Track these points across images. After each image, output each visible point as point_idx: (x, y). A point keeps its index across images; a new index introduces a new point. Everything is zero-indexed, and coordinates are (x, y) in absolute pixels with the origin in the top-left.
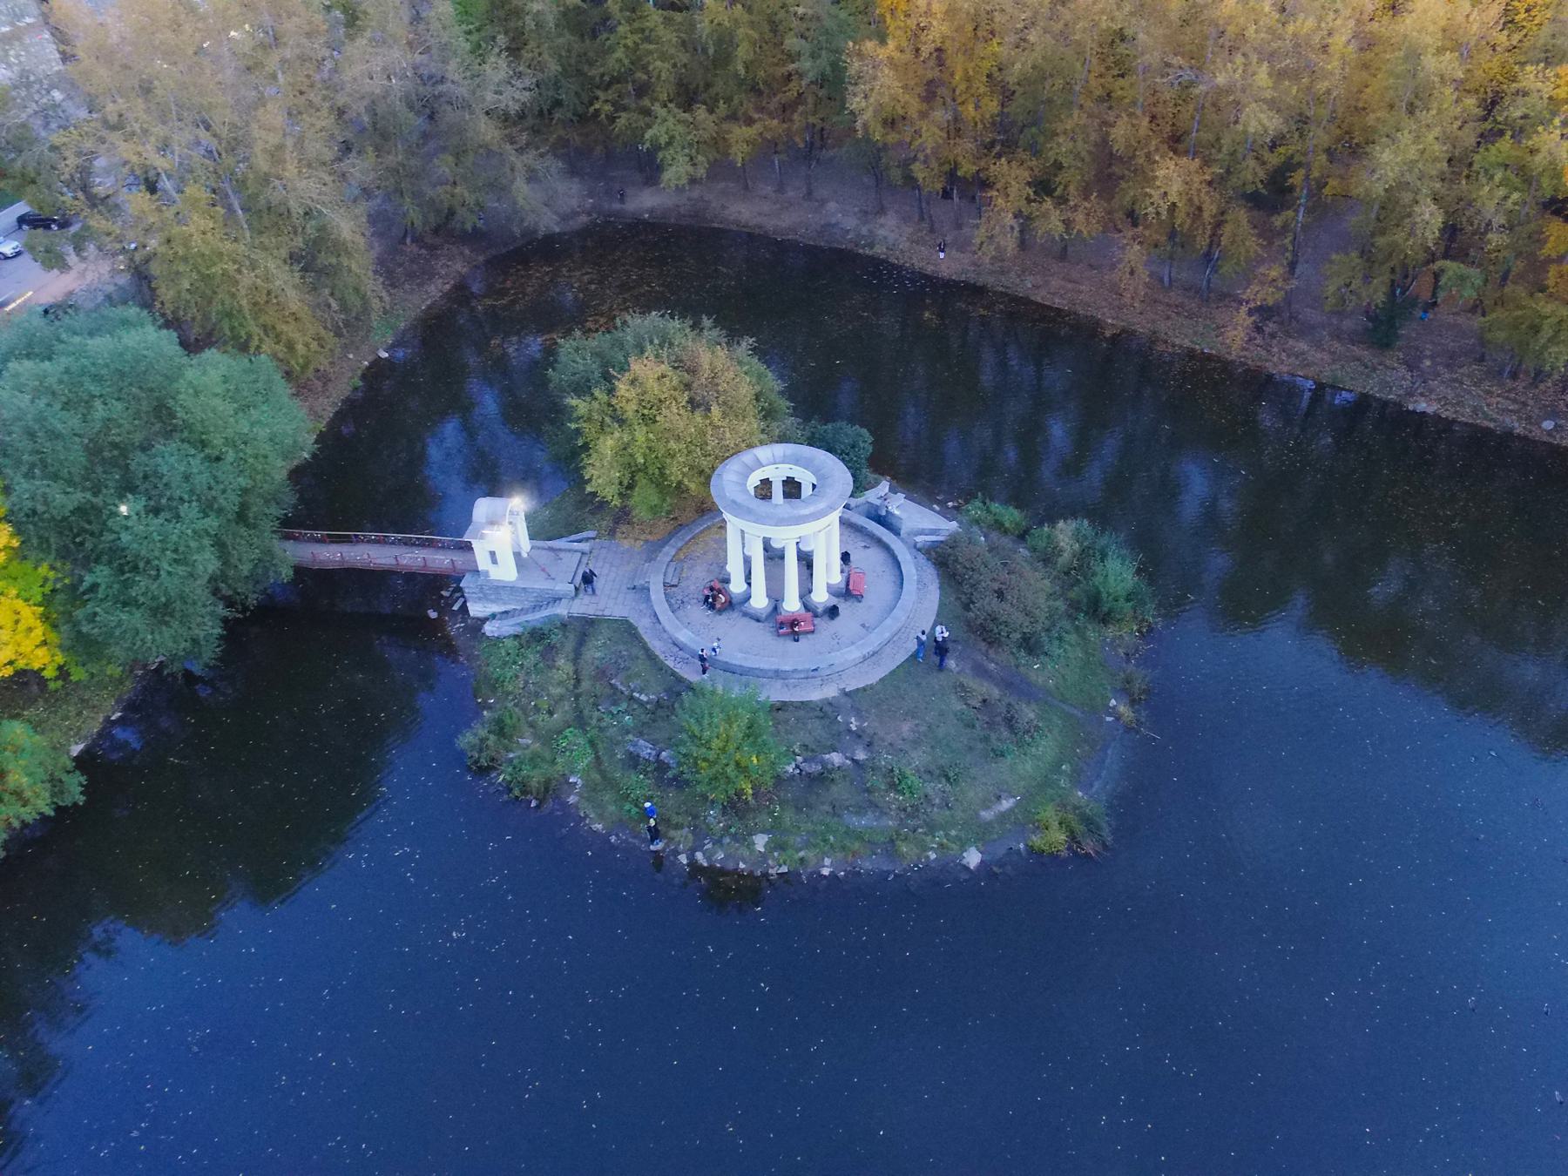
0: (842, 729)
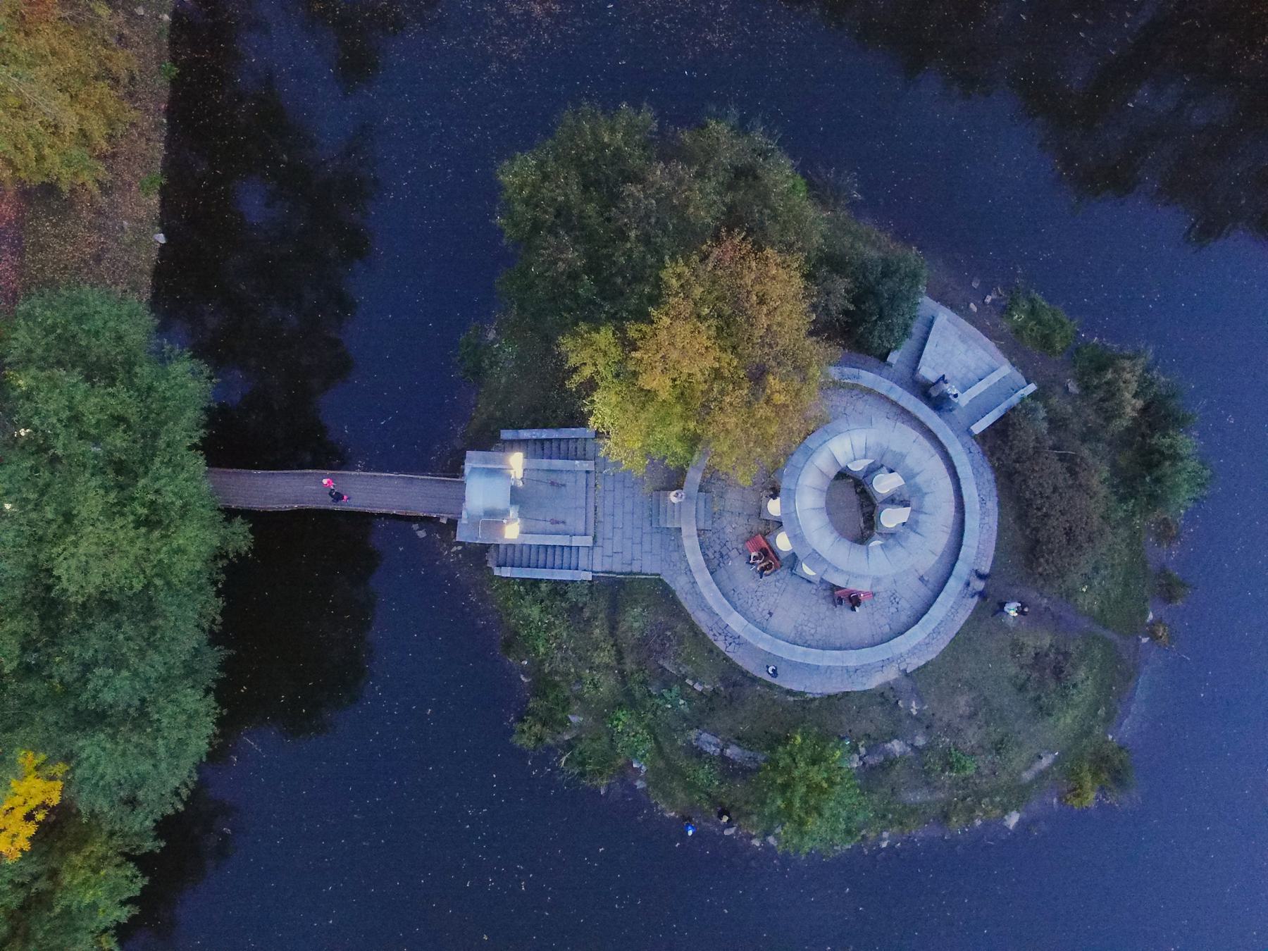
0: (903, 713)
